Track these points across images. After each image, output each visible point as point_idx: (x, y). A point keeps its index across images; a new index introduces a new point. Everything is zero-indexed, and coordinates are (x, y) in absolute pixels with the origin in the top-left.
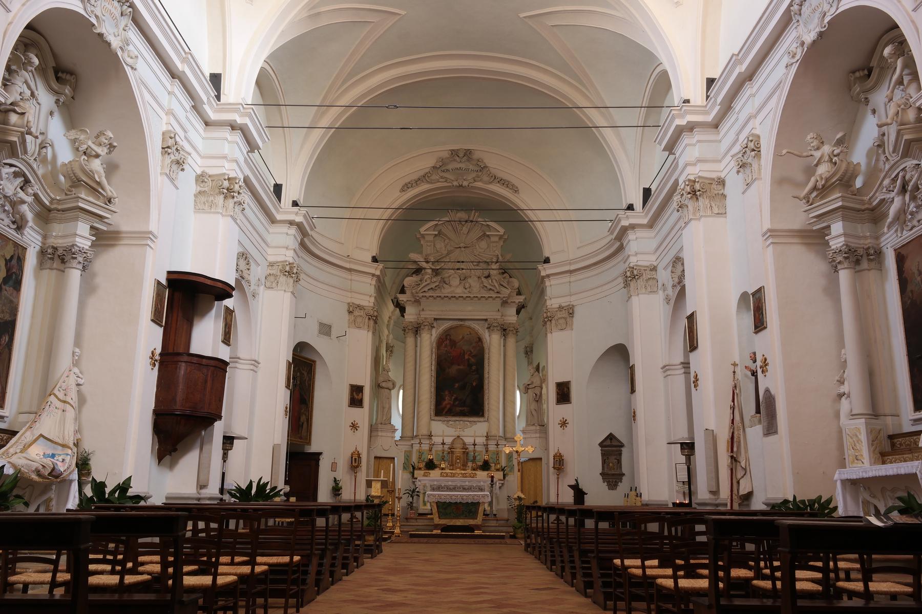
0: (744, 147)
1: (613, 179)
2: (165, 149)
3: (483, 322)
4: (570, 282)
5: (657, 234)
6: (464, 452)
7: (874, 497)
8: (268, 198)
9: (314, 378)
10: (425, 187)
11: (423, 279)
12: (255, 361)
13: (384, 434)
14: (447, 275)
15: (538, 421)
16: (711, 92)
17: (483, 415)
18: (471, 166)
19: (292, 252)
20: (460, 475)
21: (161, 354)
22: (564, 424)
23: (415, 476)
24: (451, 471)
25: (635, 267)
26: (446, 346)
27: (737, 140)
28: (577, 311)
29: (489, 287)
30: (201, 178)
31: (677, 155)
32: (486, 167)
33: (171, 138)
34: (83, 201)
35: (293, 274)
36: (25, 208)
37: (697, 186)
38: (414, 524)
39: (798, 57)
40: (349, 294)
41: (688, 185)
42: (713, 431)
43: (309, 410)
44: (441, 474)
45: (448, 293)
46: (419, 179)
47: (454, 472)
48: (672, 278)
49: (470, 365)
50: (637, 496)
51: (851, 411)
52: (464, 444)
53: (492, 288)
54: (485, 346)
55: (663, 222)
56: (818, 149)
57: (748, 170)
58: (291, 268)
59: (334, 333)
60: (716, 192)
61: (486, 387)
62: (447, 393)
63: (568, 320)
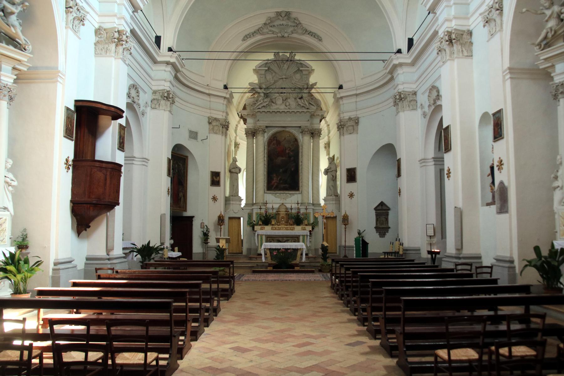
0: (490, 7)
1: (386, 31)
3: (299, 128)
4: (356, 102)
5: (418, 69)
6: (286, 214)
9: (187, 168)
10: (258, 37)
11: (258, 100)
13: (234, 202)
14: (274, 97)
15: (334, 193)
17: (298, 190)
18: (290, 23)
19: (169, 83)
20: (284, 229)
21: (73, 161)
22: (351, 195)
23: (255, 230)
24: (278, 226)
25: (402, 93)
26: (274, 145)
28: (361, 121)
29: (302, 105)
30: (98, 32)
31: (438, 13)
32: (300, 23)
35: (170, 98)
37: (453, 36)
38: (255, 261)
40: (209, 111)
41: (446, 35)
42: (460, 208)
43: (184, 189)
44: (272, 228)
45: (275, 109)
46: (255, 32)
47: (280, 226)
48: (429, 100)
49: (290, 157)
50: (401, 245)
52: (287, 208)
54: (300, 144)
55: (421, 63)
56: (548, 9)
57: (492, 24)
58: (168, 94)
59: (200, 137)
60: (466, 40)
61: (300, 171)
62: (275, 175)
63: (355, 127)
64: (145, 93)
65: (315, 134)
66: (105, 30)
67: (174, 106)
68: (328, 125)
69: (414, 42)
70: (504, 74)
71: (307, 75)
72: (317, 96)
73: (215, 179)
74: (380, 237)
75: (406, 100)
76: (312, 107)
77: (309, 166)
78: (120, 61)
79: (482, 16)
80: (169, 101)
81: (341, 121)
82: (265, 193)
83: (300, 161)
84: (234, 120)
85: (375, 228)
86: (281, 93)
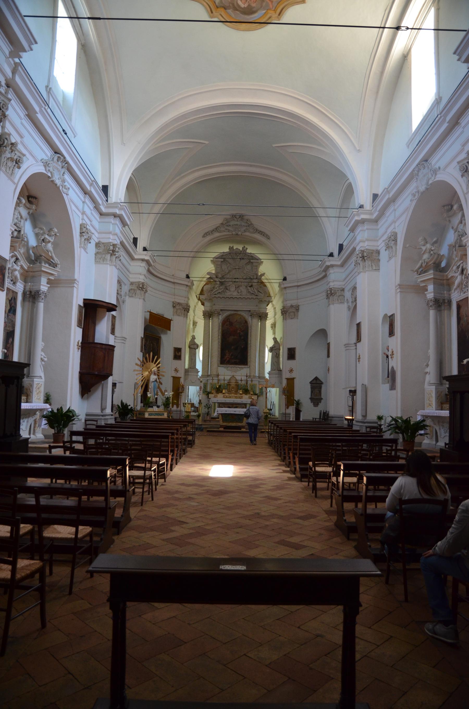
2: (81, 233)
4: (297, 292)
6: (236, 385)
7: (435, 424)
8: (130, 246)
12: (124, 338)
13: (192, 374)
14: (228, 285)
16: (374, 204)
17: (247, 364)
19: (143, 276)
21: (82, 343)
23: (209, 397)
27: (386, 232)
29: (252, 292)
30: (98, 245)
31: (356, 234)
32: (252, 224)
33: (85, 227)
34: (44, 267)
35: (144, 289)
36: (17, 273)
37: (365, 254)
39: (416, 197)
46: (213, 230)
47: (230, 395)
51: (430, 382)
52: (236, 380)
53: (253, 293)
54: (249, 326)
55: (348, 266)
56: (424, 245)
58: (143, 286)
61: (249, 349)
62: (227, 351)
63: (296, 313)
64: (125, 285)
65: (263, 317)
66: (103, 243)
67: (147, 294)
68: (275, 308)
69: (344, 247)
70: (396, 288)
71: (257, 266)
72: (265, 281)
73: (177, 354)
74: (314, 406)
75: (336, 295)
76: (260, 294)
77: (256, 344)
78: (114, 267)
79: (385, 242)
80: (143, 290)
81: (284, 307)
82: (218, 366)
83: (249, 340)
84: (193, 302)
85: (310, 398)
86: (235, 282)
